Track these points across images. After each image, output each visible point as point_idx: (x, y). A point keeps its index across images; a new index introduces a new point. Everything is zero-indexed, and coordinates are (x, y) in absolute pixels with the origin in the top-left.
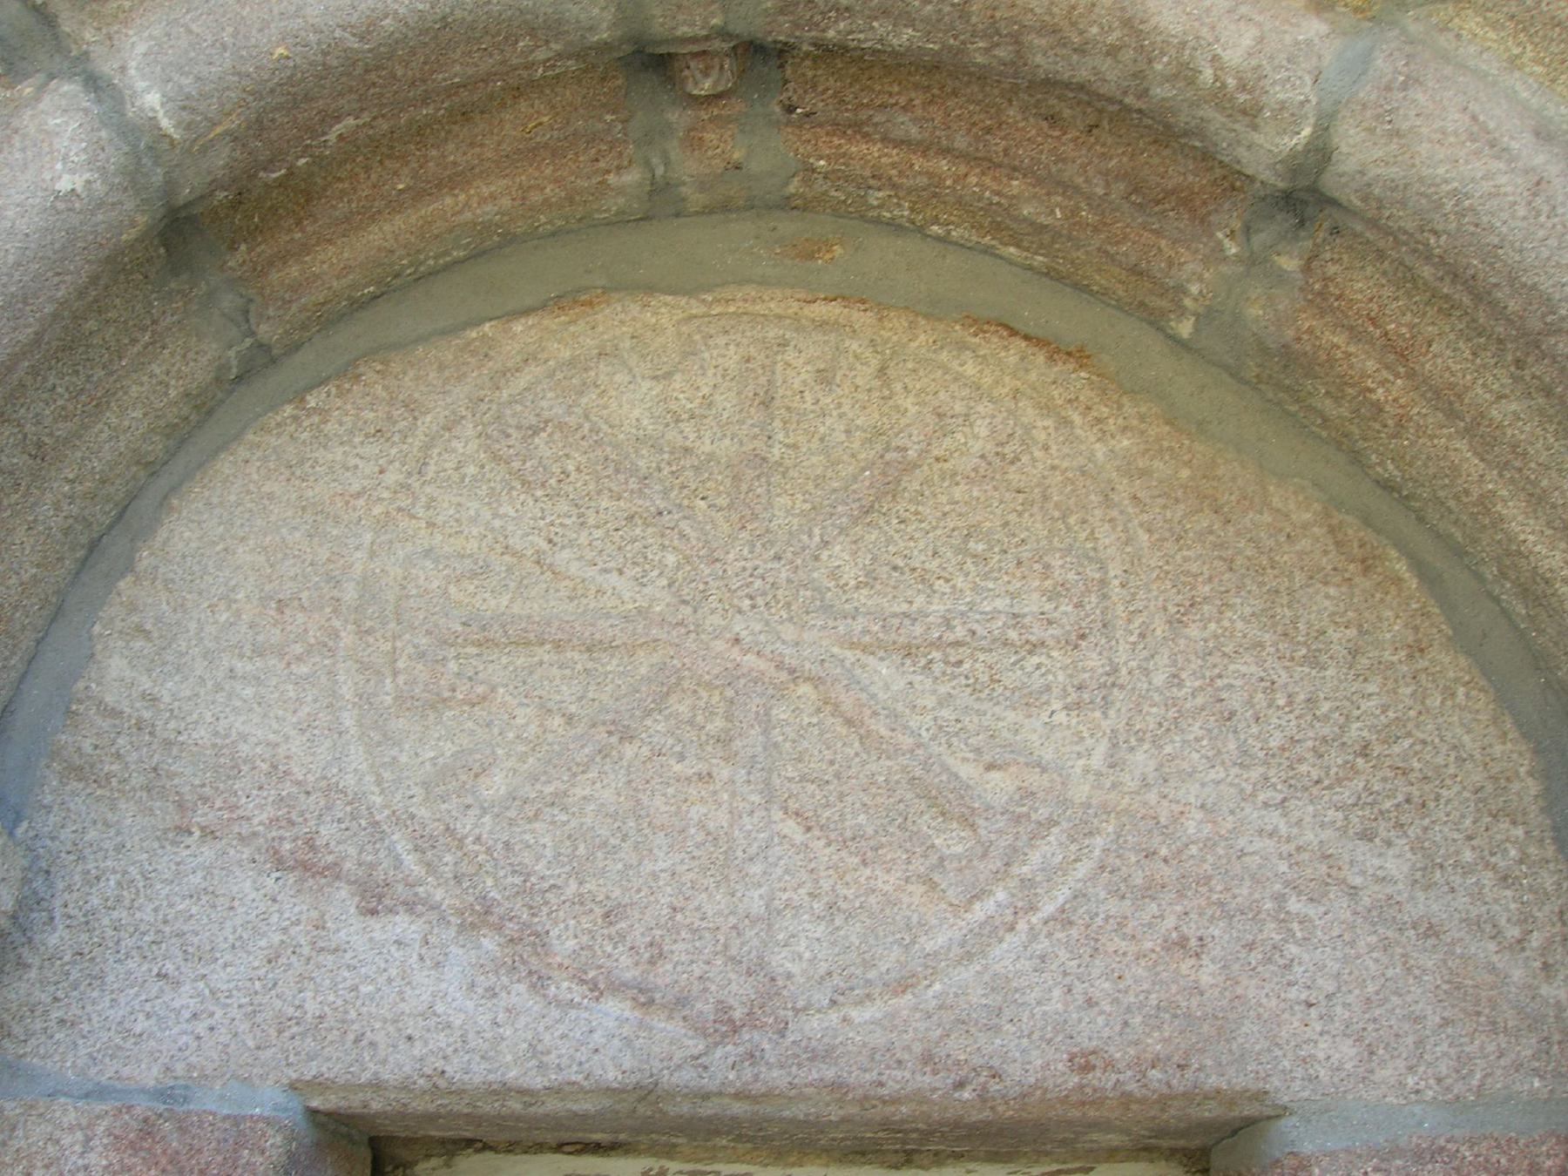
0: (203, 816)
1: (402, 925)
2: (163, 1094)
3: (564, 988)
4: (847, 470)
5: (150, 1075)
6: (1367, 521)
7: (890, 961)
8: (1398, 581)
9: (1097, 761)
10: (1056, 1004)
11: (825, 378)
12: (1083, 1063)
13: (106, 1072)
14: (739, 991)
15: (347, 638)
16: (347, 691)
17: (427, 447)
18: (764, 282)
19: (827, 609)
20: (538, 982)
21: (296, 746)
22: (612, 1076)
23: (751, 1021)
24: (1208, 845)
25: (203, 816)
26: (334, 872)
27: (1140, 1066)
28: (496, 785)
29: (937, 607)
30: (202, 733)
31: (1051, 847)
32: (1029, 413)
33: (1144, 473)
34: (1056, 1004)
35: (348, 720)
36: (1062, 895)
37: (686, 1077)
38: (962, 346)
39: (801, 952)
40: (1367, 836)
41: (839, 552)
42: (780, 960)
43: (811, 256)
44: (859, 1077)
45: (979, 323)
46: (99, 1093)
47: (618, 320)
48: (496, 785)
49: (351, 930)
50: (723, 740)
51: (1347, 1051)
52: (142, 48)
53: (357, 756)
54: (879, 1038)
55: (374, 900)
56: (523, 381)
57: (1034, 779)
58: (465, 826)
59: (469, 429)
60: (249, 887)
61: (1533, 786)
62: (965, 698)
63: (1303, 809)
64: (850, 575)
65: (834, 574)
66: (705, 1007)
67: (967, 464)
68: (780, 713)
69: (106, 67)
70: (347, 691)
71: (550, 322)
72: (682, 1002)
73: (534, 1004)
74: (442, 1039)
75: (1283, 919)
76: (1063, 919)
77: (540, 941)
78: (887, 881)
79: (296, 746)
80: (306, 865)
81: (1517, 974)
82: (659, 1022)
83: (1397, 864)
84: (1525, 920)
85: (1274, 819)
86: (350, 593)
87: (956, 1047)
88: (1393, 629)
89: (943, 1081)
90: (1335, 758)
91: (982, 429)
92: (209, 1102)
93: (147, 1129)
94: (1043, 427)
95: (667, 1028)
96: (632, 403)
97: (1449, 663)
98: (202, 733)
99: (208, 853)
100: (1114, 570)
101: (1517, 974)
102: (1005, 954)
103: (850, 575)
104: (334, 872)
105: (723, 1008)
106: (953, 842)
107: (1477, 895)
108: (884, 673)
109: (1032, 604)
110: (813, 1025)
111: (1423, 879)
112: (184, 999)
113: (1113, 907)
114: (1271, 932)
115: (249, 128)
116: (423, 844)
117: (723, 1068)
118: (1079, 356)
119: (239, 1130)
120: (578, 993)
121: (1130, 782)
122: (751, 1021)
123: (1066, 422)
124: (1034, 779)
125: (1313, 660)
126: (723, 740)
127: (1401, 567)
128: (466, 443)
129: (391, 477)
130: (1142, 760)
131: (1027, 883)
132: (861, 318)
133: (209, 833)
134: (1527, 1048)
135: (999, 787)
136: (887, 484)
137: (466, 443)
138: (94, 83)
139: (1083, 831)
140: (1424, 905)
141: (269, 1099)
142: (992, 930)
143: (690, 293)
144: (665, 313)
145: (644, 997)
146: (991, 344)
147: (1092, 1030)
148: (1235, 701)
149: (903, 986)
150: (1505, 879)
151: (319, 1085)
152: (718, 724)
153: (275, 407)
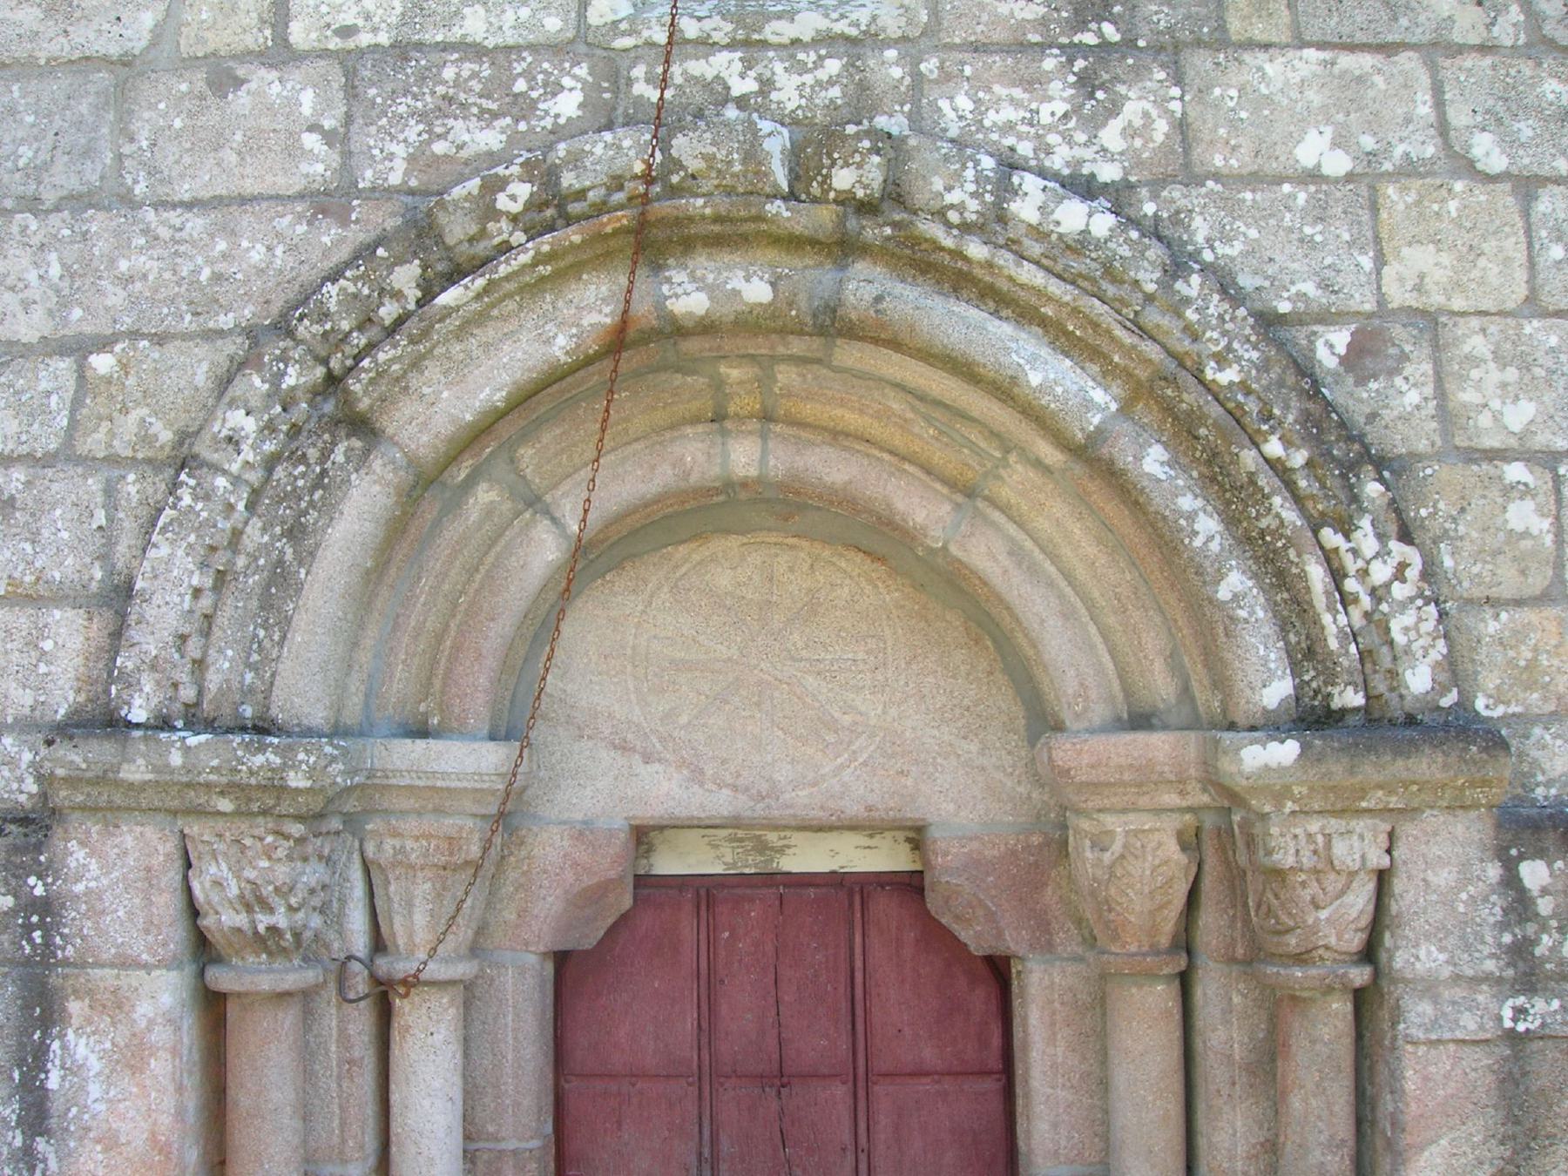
0: (587, 732)
1: (656, 766)
2: (585, 822)
3: (709, 786)
4: (799, 605)
5: (579, 816)
6: (980, 625)
7: (811, 776)
8: (987, 648)
9: (879, 711)
10: (861, 791)
11: (791, 569)
12: (869, 809)
13: (566, 816)
14: (765, 787)
15: (629, 668)
16: (631, 687)
17: (652, 596)
18: (769, 530)
19: (793, 659)
20: (701, 784)
21: (616, 707)
22: (726, 813)
23: (768, 796)
24: (913, 740)
25: (587, 732)
26: (633, 750)
27: (887, 810)
28: (684, 719)
29: (829, 657)
30: (583, 703)
31: (862, 741)
32: (864, 584)
33: (903, 607)
34: (861, 791)
35: (633, 697)
36: (865, 756)
37: (749, 813)
38: (841, 555)
39: (783, 774)
40: (965, 738)
41: (796, 636)
42: (777, 776)
43: (786, 520)
44: (801, 813)
45: (847, 546)
46: (565, 823)
47: (718, 545)
48: (684, 719)
49: (641, 769)
50: (758, 704)
51: (951, 807)
52: (568, 507)
53: (637, 710)
54: (806, 801)
55: (647, 759)
56: (684, 570)
57: (859, 718)
58: (675, 734)
59: (666, 589)
60: (606, 756)
61: (1023, 722)
62: (837, 689)
63: (945, 729)
64: (800, 644)
65: (794, 644)
66: (754, 791)
67: (842, 603)
68: (776, 694)
69: (558, 515)
70: (631, 687)
71: (693, 545)
72: (747, 789)
73: (701, 791)
74: (672, 803)
75: (935, 765)
76: (865, 764)
77: (702, 772)
78: (810, 751)
79: (616, 707)
80: (624, 748)
81: (1009, 784)
82: (740, 796)
83: (974, 747)
84: (1014, 766)
85: (936, 732)
86: (629, 652)
87: (831, 804)
88: (984, 665)
89: (827, 814)
90: (958, 711)
91: (846, 590)
92: (602, 823)
93: (581, 833)
94: (868, 589)
95: (742, 797)
96: (723, 579)
97: (1000, 678)
98: (583, 703)
99: (590, 744)
100: (889, 644)
101: (1009, 784)
102: (847, 775)
103: (800, 644)
104: (633, 750)
105: (759, 792)
106: (831, 738)
107: (1000, 758)
108: (810, 680)
109: (861, 656)
110: (787, 796)
111: (982, 753)
112: (588, 792)
113: (881, 760)
114: (931, 769)
115: (466, 200)
116: (662, 740)
117: (759, 810)
118: (881, 559)
119: (611, 834)
120: (714, 788)
121: (889, 719)
122: (768, 796)
123: (876, 586)
124: (859, 718)
125: (953, 677)
126: (758, 704)
127: (989, 643)
128: (665, 594)
129: (640, 608)
130: (893, 712)
131: (854, 752)
132: (805, 544)
133: (590, 737)
134: (1009, 806)
135: (847, 720)
136: (812, 608)
137: (665, 594)
138: (554, 520)
139: (872, 736)
140: (984, 761)
141: (619, 823)
142: (842, 767)
143: (743, 534)
144: (734, 541)
145: (735, 788)
146: (851, 554)
147: (872, 799)
148: (925, 691)
149: (815, 784)
150: (1009, 753)
151: (634, 817)
152: (755, 699)
153: (594, 580)
